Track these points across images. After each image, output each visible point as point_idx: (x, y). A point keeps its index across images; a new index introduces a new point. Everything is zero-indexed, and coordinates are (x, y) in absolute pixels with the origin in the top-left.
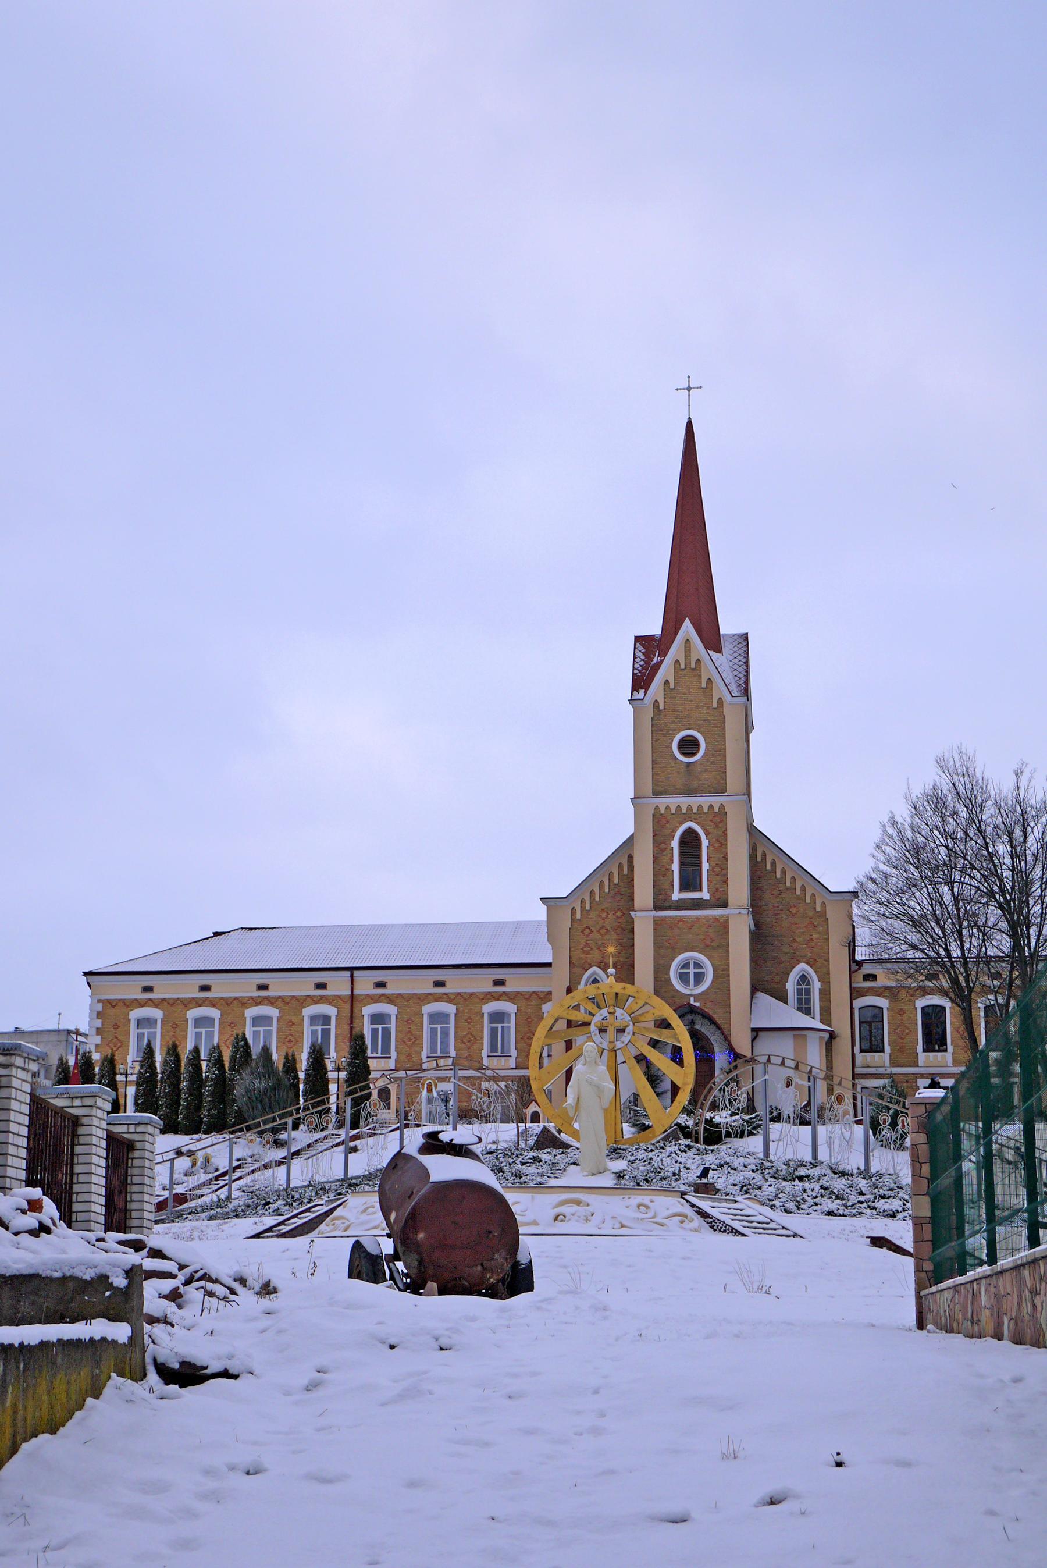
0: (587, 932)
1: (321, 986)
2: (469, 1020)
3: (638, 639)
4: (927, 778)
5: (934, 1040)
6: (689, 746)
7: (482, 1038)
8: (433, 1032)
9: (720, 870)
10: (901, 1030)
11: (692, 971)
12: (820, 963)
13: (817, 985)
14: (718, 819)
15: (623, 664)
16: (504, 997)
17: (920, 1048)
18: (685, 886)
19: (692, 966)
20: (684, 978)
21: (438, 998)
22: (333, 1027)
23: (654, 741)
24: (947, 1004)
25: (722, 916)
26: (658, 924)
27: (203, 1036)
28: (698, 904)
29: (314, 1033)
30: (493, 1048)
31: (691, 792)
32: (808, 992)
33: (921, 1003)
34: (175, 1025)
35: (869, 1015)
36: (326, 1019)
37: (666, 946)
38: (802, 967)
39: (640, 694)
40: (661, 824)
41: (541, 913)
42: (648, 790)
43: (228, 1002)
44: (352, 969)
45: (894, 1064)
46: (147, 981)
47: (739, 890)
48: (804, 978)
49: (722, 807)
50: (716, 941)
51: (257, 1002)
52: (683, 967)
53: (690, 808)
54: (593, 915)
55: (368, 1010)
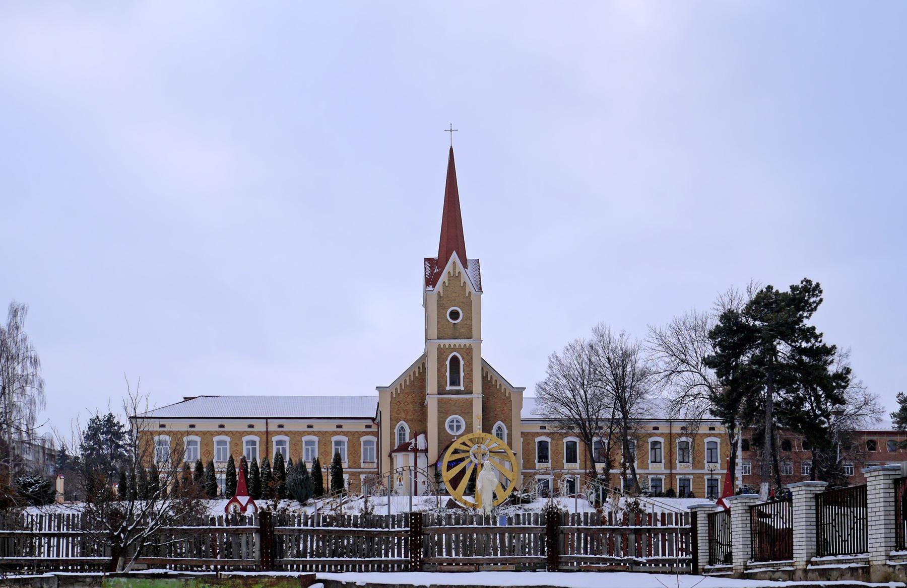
1: (251, 426)
2: (325, 444)
4: (588, 337)
5: (571, 458)
6: (454, 315)
8: (219, 450)
10: (556, 453)
11: (455, 424)
12: (508, 421)
13: (506, 432)
14: (468, 352)
15: (419, 273)
17: (649, 461)
18: (452, 384)
20: (451, 427)
21: (309, 434)
22: (257, 446)
23: (438, 312)
24: (577, 440)
26: (440, 401)
27: (252, 451)
28: (458, 392)
29: (278, 449)
31: (455, 338)
33: (538, 439)
34: (296, 445)
35: (684, 446)
36: (254, 443)
37: (444, 412)
38: (499, 422)
39: (431, 288)
40: (442, 353)
41: (377, 393)
42: (434, 334)
46: (163, 422)
47: (477, 386)
49: (470, 345)
51: (219, 433)
55: (275, 439)
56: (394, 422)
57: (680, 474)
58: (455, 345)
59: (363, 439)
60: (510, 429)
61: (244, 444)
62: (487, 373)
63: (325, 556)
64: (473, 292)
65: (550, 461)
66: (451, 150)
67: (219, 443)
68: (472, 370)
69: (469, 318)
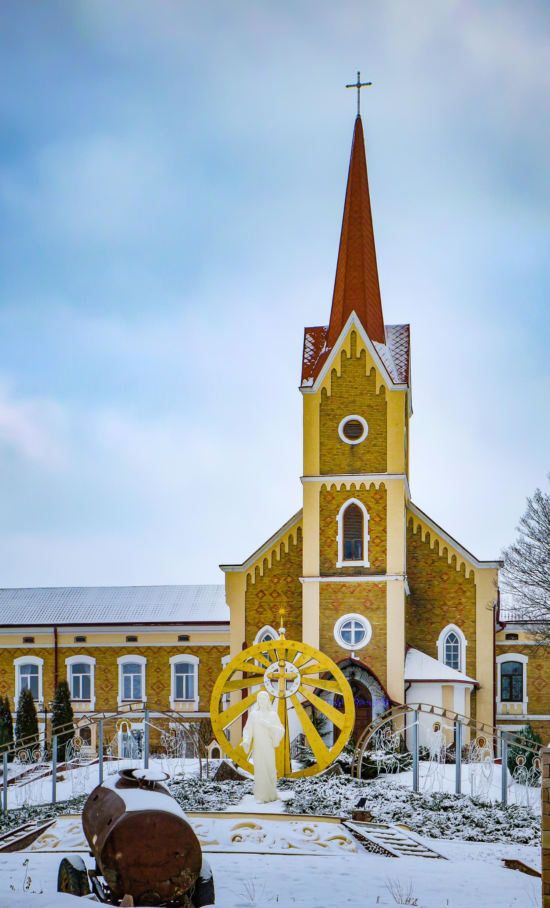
0: (261, 595)
2: (158, 670)
3: (307, 330)
6: (354, 429)
7: (169, 686)
9: (380, 541)
11: (353, 629)
14: (379, 495)
16: (188, 651)
18: (349, 555)
19: (353, 625)
20: (345, 635)
21: (131, 651)
22: (40, 675)
23: (322, 425)
25: (381, 582)
26: (323, 589)
28: (359, 572)
30: (179, 694)
32: (456, 649)
36: (34, 669)
37: (331, 605)
40: (328, 499)
41: (220, 578)
45: (531, 711)
48: (452, 637)
49: (382, 485)
50: (374, 603)
52: (345, 626)
53: (353, 485)
54: (266, 580)
56: (252, 628)
58: (363, 485)
59: (122, 660)
60: (472, 637)
61: (17, 671)
65: (526, 699)
66: (358, 122)
67: (128, 668)
68: (385, 531)
69: (380, 434)
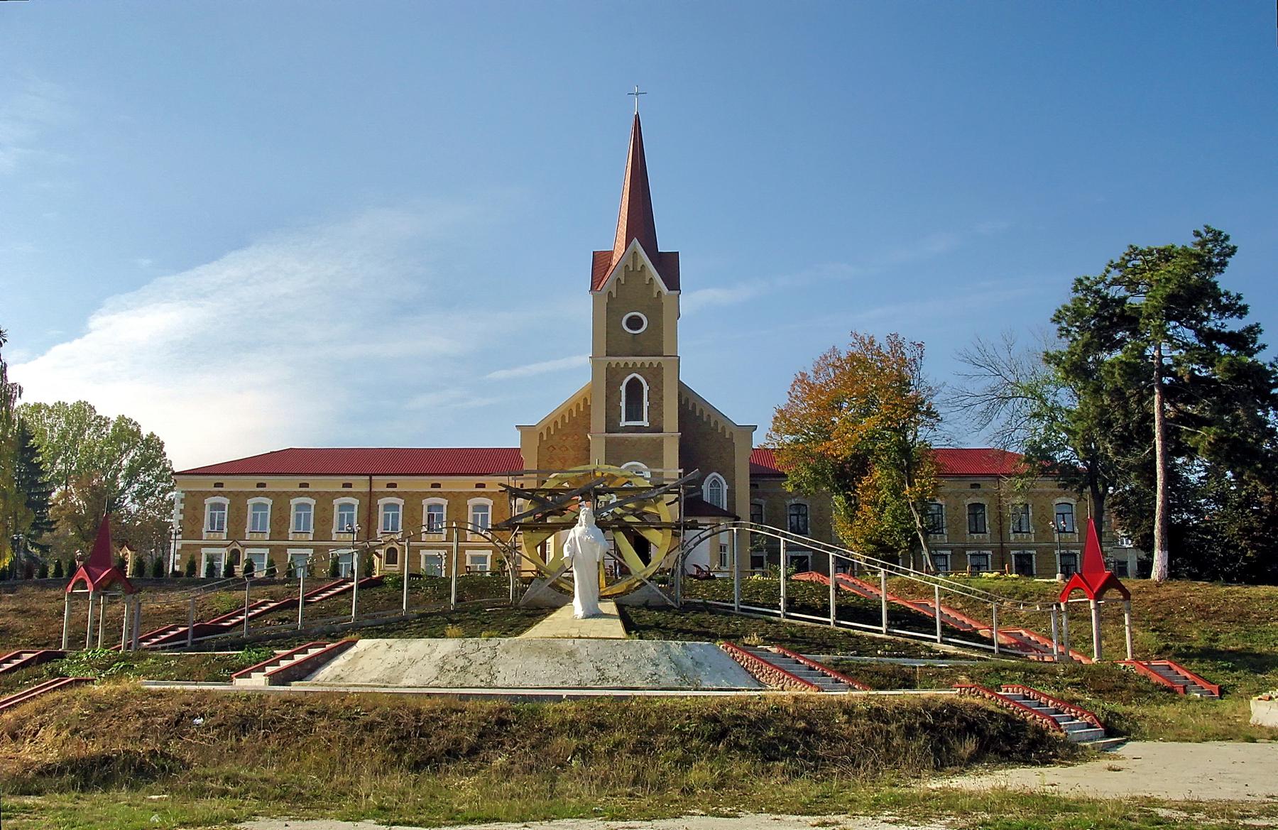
6: (635, 323)
9: (657, 407)
14: (655, 375)
26: (608, 442)
40: (612, 377)
43: (238, 494)
44: (371, 475)
47: (671, 419)
48: (715, 482)
53: (634, 364)
55: (381, 502)
57: (970, 549)
60: (731, 482)
62: (687, 400)
63: (1168, 509)
64: (665, 290)
66: (637, 117)
69: (656, 326)
